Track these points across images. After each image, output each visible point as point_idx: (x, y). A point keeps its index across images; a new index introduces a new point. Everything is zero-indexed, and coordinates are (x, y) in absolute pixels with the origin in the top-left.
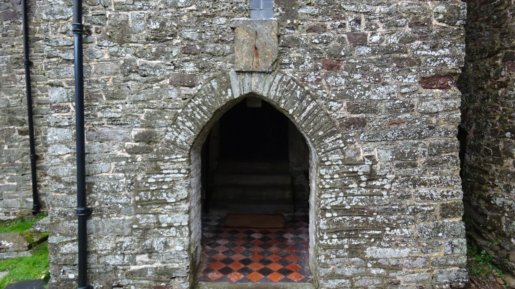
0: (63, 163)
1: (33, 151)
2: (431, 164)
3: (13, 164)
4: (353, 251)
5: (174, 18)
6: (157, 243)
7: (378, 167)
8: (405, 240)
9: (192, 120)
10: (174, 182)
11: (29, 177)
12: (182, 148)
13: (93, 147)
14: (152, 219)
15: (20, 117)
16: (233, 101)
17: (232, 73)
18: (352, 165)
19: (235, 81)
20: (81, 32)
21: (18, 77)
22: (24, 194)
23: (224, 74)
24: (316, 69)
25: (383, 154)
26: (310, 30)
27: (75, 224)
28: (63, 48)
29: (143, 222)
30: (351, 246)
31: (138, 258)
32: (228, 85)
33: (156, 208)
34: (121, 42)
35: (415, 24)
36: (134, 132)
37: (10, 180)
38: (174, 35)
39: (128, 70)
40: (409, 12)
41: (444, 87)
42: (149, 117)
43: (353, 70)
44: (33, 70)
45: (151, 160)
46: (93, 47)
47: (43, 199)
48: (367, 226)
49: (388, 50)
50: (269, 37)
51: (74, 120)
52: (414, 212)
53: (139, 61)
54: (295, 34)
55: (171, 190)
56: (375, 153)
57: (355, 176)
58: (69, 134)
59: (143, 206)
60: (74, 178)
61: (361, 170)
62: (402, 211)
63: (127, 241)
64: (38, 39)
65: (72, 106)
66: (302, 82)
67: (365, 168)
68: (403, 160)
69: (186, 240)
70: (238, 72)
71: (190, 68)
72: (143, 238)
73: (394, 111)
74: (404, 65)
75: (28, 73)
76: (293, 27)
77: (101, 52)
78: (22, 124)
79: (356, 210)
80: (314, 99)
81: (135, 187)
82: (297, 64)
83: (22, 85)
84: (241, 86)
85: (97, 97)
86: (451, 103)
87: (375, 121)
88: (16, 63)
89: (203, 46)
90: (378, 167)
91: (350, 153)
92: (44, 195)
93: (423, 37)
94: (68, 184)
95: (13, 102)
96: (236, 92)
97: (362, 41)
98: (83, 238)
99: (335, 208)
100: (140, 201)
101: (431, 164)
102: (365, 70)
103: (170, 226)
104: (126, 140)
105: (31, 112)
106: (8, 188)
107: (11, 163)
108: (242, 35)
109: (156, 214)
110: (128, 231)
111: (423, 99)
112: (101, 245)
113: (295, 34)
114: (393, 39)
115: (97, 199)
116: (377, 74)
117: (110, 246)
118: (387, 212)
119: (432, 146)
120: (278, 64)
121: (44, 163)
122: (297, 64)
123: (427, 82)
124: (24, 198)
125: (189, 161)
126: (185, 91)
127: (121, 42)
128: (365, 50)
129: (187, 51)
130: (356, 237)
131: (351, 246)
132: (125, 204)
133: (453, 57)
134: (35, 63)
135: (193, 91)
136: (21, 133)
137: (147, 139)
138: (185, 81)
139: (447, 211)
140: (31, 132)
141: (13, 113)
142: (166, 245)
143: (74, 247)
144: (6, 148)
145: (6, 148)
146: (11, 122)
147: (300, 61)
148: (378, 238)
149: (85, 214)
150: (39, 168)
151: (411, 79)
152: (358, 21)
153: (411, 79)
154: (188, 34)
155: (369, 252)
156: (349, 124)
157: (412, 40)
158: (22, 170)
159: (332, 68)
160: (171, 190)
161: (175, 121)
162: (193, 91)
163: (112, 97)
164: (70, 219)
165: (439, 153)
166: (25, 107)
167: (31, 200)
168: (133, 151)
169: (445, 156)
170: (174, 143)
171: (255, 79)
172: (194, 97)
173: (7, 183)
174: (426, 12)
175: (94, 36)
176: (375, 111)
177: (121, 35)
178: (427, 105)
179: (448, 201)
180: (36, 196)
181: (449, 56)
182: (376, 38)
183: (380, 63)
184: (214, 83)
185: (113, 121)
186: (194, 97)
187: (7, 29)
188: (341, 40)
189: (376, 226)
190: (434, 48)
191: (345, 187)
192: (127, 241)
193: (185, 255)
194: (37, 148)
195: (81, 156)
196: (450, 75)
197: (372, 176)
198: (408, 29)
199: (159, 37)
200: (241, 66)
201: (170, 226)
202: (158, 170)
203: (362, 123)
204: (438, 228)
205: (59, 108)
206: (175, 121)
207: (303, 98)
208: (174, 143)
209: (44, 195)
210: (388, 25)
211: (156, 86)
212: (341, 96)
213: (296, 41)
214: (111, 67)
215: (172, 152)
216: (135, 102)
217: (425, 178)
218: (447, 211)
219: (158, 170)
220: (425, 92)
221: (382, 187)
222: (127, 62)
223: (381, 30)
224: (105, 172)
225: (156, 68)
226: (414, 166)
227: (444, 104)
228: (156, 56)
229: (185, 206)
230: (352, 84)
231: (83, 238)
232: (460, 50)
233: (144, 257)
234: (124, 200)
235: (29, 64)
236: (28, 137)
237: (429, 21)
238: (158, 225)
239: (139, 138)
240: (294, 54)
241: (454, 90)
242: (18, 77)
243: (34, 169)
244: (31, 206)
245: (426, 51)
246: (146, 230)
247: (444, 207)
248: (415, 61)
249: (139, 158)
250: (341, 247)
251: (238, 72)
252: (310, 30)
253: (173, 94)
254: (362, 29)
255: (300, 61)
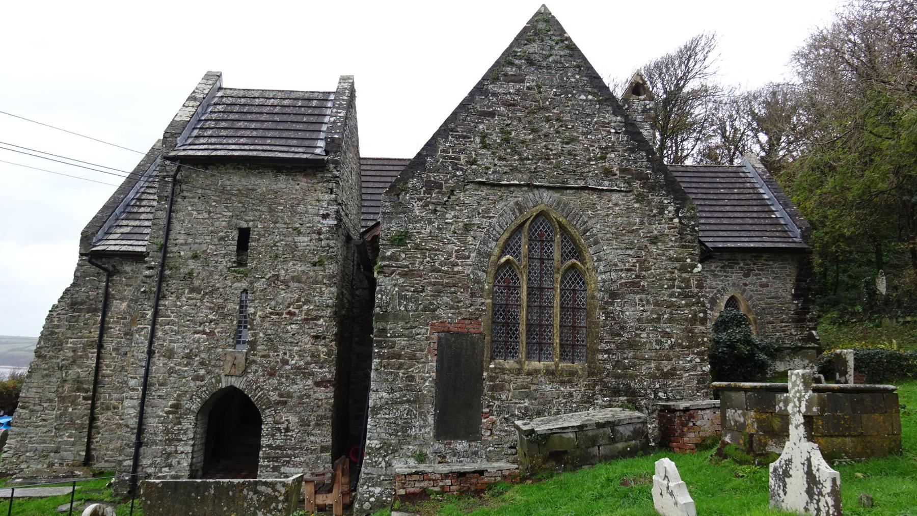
0: (131, 418)
1: (92, 413)
2: (317, 425)
3: (74, 424)
4: (276, 469)
5: (197, 348)
6: (174, 462)
7: (291, 425)
8: (301, 463)
9: (200, 398)
10: (187, 429)
11: (85, 434)
12: (193, 412)
13: (148, 410)
14: (173, 449)
15: (85, 386)
16: (222, 389)
17: (223, 376)
18: (278, 424)
19: (224, 380)
20: (150, 353)
21: (90, 355)
22: (78, 448)
23: (219, 375)
24: (263, 375)
25: (294, 419)
26: (262, 356)
27: (133, 450)
28: (140, 360)
29: (168, 450)
30: (274, 466)
31: (163, 469)
32: (220, 381)
33: (176, 443)
34: (169, 358)
35: (313, 356)
36: (170, 403)
37: (68, 437)
38: (196, 356)
39: (171, 371)
40: (310, 351)
41: (326, 387)
42: (179, 396)
43: (281, 377)
44: (103, 351)
45: (177, 418)
46: (155, 360)
47: (94, 453)
48: (283, 456)
49: (299, 368)
50: (241, 359)
51: (140, 396)
52: (307, 450)
53: (178, 368)
54: (255, 358)
55: (185, 433)
56: (290, 418)
57: (279, 430)
58: (136, 403)
59: (169, 442)
60: (136, 426)
61: (282, 426)
62: (301, 448)
63: (159, 460)
64: (111, 328)
65: (140, 389)
66: (256, 382)
67: (284, 426)
68: (304, 423)
69: (190, 460)
70: (226, 375)
71: (202, 372)
72: (167, 458)
73: (301, 397)
74: (307, 375)
75: (99, 353)
76: (254, 355)
77: (159, 362)
78: (87, 391)
79: (278, 447)
80: (262, 390)
81: (167, 431)
82: (255, 373)
83: (92, 362)
84: (227, 382)
85: (153, 385)
86: (329, 395)
87: (291, 402)
88: (91, 345)
89: (209, 362)
90: (291, 425)
91: (277, 418)
92: (95, 449)
93: (316, 363)
94: (132, 429)
95: (83, 375)
96: (223, 385)
97: (287, 363)
98: (136, 458)
99: (268, 446)
100: (168, 439)
101: (317, 425)
102: (287, 377)
103: (182, 453)
104: (165, 407)
105: (96, 383)
106: (67, 443)
107: (72, 422)
108: (229, 358)
109: (176, 446)
110: (160, 455)
111: (315, 392)
112: (145, 462)
113: (255, 358)
114: (302, 363)
115: (147, 437)
116: (293, 379)
117: (149, 462)
118: (293, 449)
119: (319, 416)
120: (245, 372)
121: (99, 423)
122: (255, 373)
123: (318, 384)
124: (78, 452)
125: (196, 419)
126: (198, 383)
127: (169, 358)
128: (288, 367)
129: (202, 363)
130: (276, 461)
131: (274, 466)
132: (160, 441)
133: (330, 372)
134: (105, 345)
135: (203, 383)
136: (85, 398)
137: (176, 407)
138: (197, 378)
139: (323, 449)
140: (94, 398)
141: (82, 383)
142: (179, 463)
143: (129, 463)
144: (70, 410)
145: (70, 410)
146: (78, 390)
147: (256, 371)
148: (288, 462)
149: (139, 444)
150: (95, 428)
151: (310, 382)
152: (285, 354)
153: (310, 382)
154: (203, 355)
155: (283, 470)
156: (278, 403)
157: (311, 363)
158: (80, 428)
159: (272, 375)
160: (185, 433)
161: (191, 398)
162: (203, 383)
163: (161, 385)
164: (131, 447)
165: (321, 419)
166: (92, 378)
167: (84, 453)
168: (168, 413)
169: (324, 421)
170: (190, 409)
171: (234, 379)
172: (202, 387)
173: (66, 439)
174: (318, 350)
175: (157, 355)
176: (292, 397)
177: (170, 354)
178: (317, 395)
179: (324, 444)
180: (88, 450)
181: (328, 372)
182: (293, 362)
183: (294, 374)
184: (213, 380)
185: (160, 397)
186: (202, 387)
187: (89, 319)
188: (277, 362)
189: (287, 456)
190: (321, 368)
191: (273, 435)
192: (159, 460)
193: (188, 468)
194: (96, 411)
195: (141, 415)
196: (329, 381)
197: (287, 430)
198: (309, 358)
199: (189, 356)
200: (227, 373)
201: (182, 453)
202: (180, 423)
203: (284, 403)
204: (318, 458)
205: (133, 390)
206: (191, 398)
207: (256, 389)
208: (190, 409)
209: (95, 449)
210: (300, 356)
211: (184, 380)
212: (275, 389)
213: (254, 362)
214: (163, 370)
215: (188, 414)
216: (173, 388)
217: (314, 432)
218: (323, 449)
219: (180, 423)
220: (316, 389)
221: (292, 436)
222: (171, 368)
223: (296, 358)
224: (153, 424)
225: (186, 371)
226: (309, 426)
227: (325, 395)
228: (186, 366)
229: (191, 442)
230: (280, 384)
231: (136, 458)
232: (333, 369)
233: (166, 469)
234: (160, 438)
235: (100, 347)
236: (90, 402)
237: (319, 355)
238: (176, 452)
239: (172, 406)
240: (254, 368)
241: (332, 389)
242: (90, 355)
243: (91, 427)
244: (82, 459)
245: (317, 369)
246: (169, 455)
247: (322, 447)
248: (312, 374)
249: (171, 416)
250: (268, 466)
251: (226, 375)
252: (262, 356)
253: (192, 385)
254: (287, 357)
255: (256, 371)
